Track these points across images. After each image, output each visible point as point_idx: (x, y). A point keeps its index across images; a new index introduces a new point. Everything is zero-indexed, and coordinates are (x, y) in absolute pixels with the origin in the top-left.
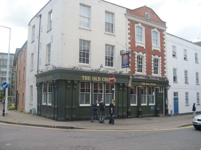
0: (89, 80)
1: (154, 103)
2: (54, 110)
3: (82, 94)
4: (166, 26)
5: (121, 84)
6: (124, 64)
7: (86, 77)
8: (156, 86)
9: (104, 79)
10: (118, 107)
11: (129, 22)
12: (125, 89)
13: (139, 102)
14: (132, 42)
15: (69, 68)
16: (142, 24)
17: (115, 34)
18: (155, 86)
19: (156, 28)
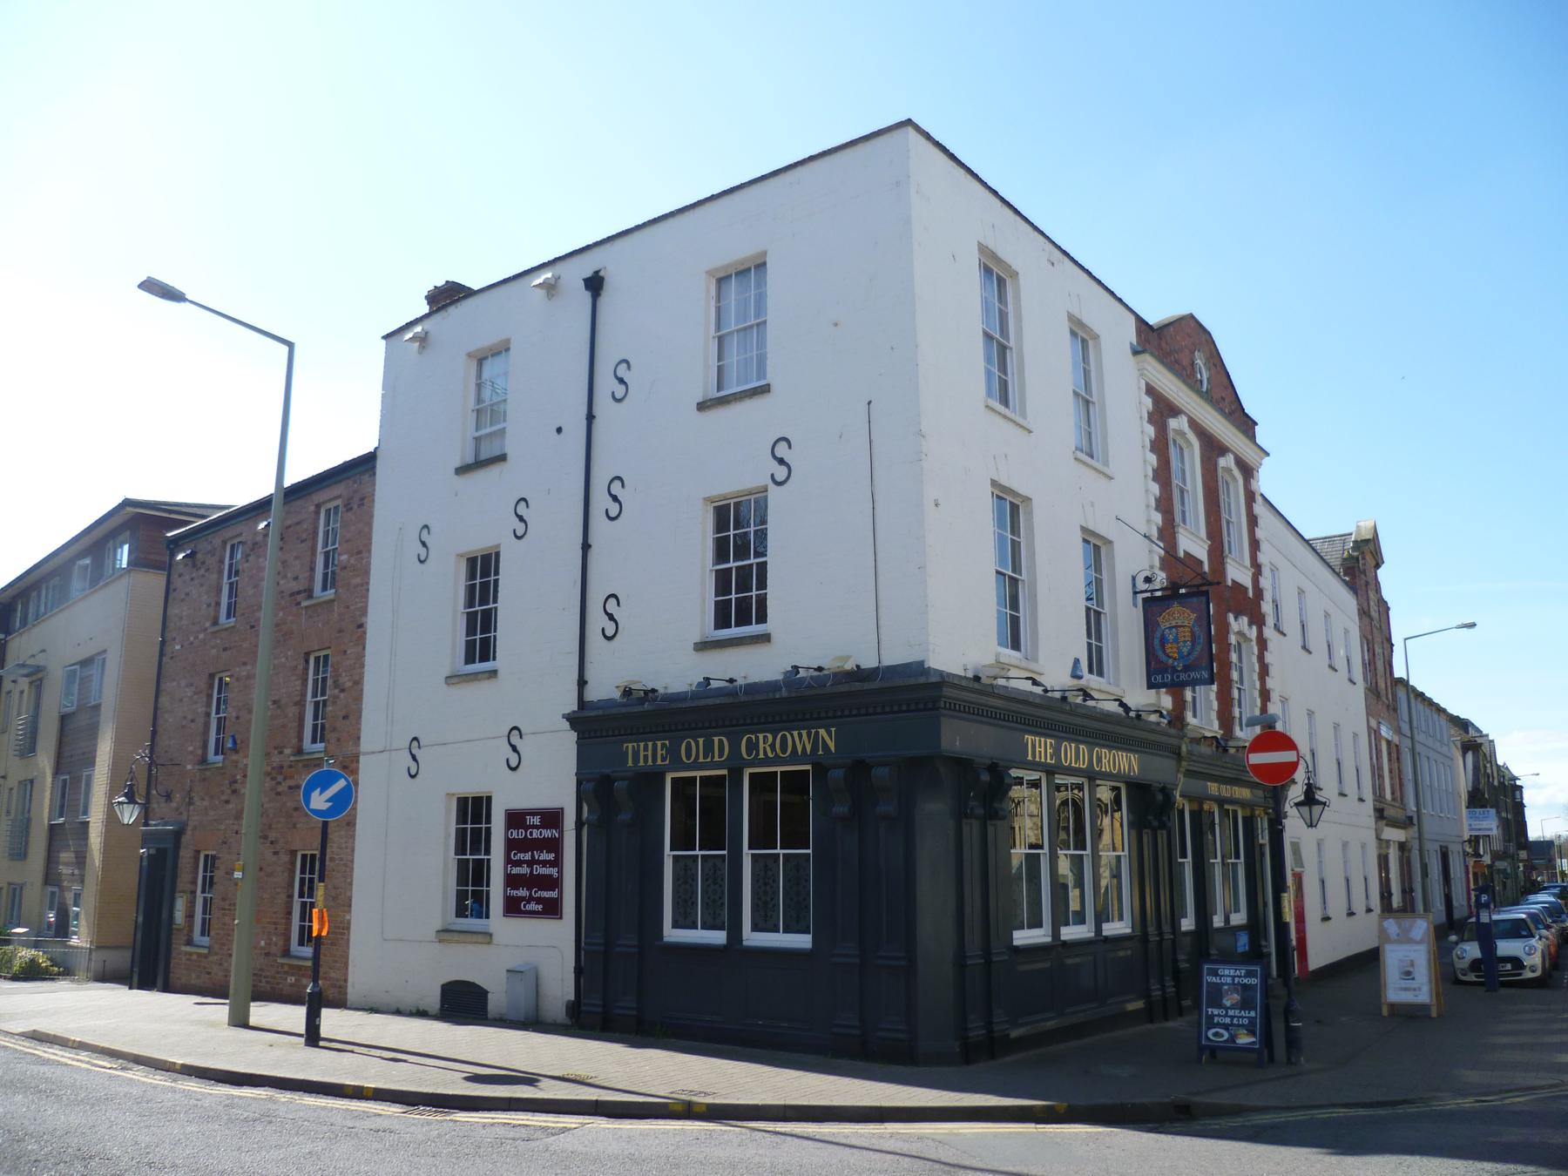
1: (1040, 925)
7: (1037, 739)
9: (1099, 760)
14: (1168, 534)
16: (1194, 425)
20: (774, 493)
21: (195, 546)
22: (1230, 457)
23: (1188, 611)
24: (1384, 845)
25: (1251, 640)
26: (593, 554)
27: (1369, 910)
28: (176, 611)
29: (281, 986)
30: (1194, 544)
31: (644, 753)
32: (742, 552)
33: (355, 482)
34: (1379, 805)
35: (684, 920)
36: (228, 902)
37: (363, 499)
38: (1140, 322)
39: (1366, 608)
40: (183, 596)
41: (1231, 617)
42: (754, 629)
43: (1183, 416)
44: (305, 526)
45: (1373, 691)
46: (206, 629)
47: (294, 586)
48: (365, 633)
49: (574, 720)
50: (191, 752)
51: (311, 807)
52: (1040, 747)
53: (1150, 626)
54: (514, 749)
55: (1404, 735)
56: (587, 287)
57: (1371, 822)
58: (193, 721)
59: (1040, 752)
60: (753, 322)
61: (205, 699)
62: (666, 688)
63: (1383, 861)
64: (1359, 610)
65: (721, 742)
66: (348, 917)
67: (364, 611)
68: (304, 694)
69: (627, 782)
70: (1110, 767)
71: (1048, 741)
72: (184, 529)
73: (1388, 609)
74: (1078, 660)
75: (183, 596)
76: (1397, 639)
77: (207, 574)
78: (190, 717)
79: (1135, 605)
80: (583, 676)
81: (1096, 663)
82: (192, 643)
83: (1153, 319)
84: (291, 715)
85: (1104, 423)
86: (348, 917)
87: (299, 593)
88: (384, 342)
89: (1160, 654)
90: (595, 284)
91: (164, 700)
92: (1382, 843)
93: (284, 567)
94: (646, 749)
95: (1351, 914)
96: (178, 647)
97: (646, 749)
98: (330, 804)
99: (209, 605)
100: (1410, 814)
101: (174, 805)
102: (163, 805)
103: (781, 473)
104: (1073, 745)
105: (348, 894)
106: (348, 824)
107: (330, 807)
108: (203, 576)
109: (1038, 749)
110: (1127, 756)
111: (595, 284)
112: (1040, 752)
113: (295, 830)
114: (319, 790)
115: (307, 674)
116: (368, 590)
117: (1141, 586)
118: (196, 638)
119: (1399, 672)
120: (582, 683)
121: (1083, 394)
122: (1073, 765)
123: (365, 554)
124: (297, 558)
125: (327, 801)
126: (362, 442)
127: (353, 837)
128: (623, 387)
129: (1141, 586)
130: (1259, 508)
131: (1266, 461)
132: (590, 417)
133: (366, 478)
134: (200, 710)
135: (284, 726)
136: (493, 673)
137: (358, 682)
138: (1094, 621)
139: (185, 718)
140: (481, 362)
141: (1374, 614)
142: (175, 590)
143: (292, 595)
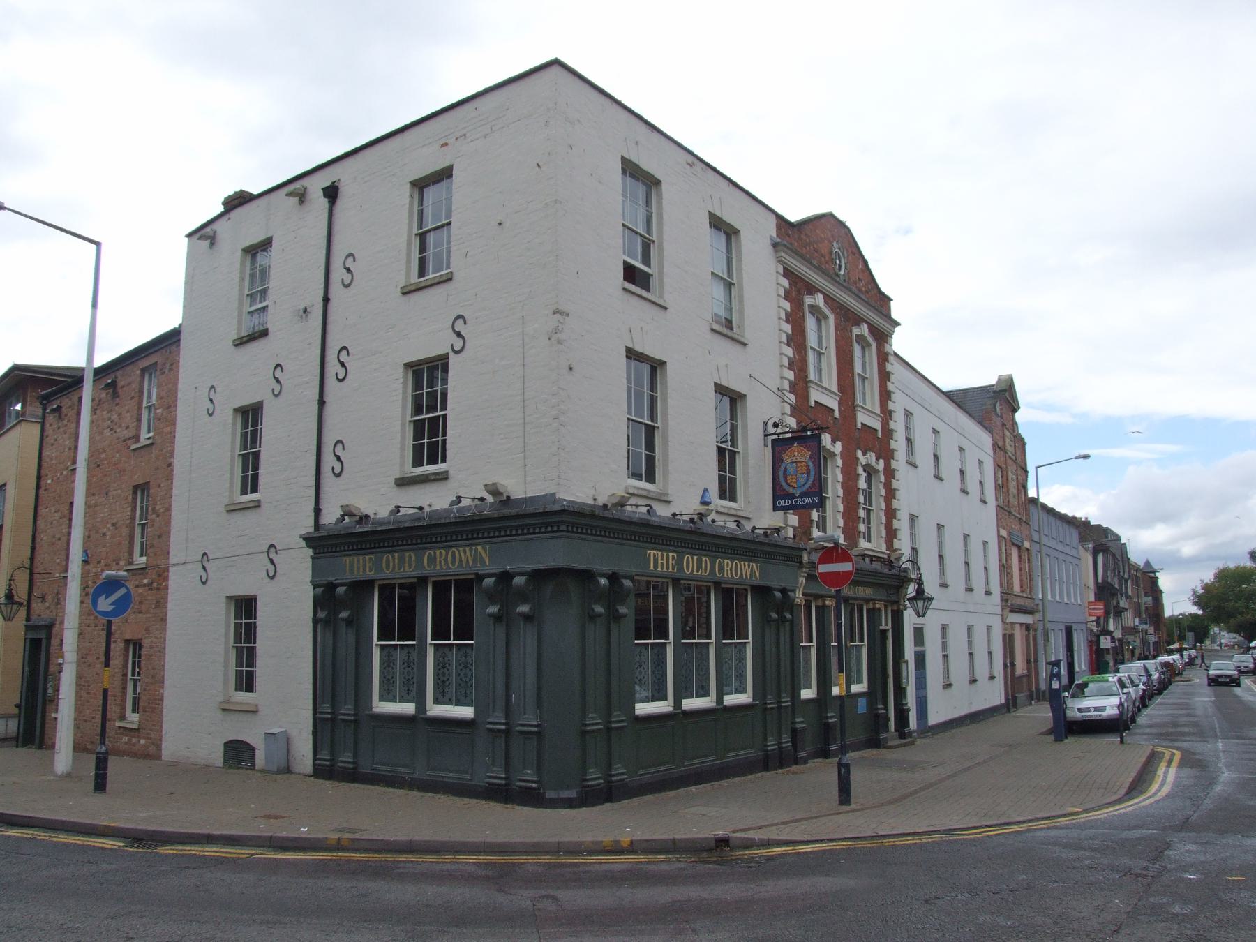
0: (670, 570)
1: (664, 698)
2: (609, 740)
3: (387, 650)
4: (894, 315)
5: (603, 575)
6: (791, 490)
7: (660, 553)
8: (873, 600)
9: (721, 568)
10: (584, 733)
11: (786, 283)
12: (622, 610)
13: (824, 685)
14: (800, 386)
15: (590, 502)
16: (827, 298)
17: (661, 296)
18: (868, 601)
19: (867, 323)
20: (453, 360)
21: (60, 403)
22: (865, 327)
23: (805, 450)
24: (1009, 626)
25: (879, 472)
26: (329, 409)
27: (992, 678)
28: (48, 453)
29: (118, 744)
30: (825, 395)
31: (360, 567)
32: (432, 408)
33: (166, 351)
34: (1005, 596)
35: (387, 695)
36: (83, 680)
37: (172, 365)
38: (780, 218)
39: (1000, 444)
40: (52, 441)
41: (859, 453)
42: (439, 467)
43: (819, 294)
44: (134, 386)
45: (1003, 510)
46: (68, 467)
47: (127, 434)
48: (172, 470)
49: (309, 540)
50: (58, 564)
51: (98, 609)
52: (662, 559)
53: (776, 461)
54: (272, 562)
55: (1035, 542)
56: (325, 196)
57: (998, 609)
58: (59, 539)
59: (662, 564)
60: (444, 222)
61: (67, 522)
62: (375, 514)
63: (1008, 640)
64: (993, 445)
65: (410, 556)
66: (161, 691)
67: (172, 455)
68: (133, 518)
69: (322, 589)
70: (731, 573)
71: (671, 555)
72: (47, 391)
73: (1024, 444)
74: (707, 490)
75: (52, 441)
76: (1030, 468)
77: (68, 424)
78: (58, 536)
79: (766, 445)
80: (318, 505)
81: (727, 489)
82: (59, 478)
83: (793, 216)
84: (124, 534)
85: (741, 302)
86: (161, 691)
87: (129, 439)
88: (187, 239)
89: (783, 483)
90: (332, 193)
91: (41, 523)
92: (1008, 626)
93: (120, 419)
94: (358, 561)
95: (973, 681)
96: (49, 481)
97: (358, 561)
98: (114, 607)
99: (70, 449)
100: (1037, 602)
101: (47, 604)
102: (39, 604)
103: (458, 344)
104: (695, 557)
105: (162, 673)
106: (162, 620)
107: (114, 609)
108: (66, 425)
109: (660, 561)
110: (749, 565)
111: (332, 193)
112: (662, 564)
113: (127, 624)
114: (104, 596)
115: (136, 503)
116: (174, 437)
117: (771, 430)
118: (62, 474)
119: (1032, 493)
120: (318, 511)
121: (725, 277)
122: (695, 573)
123: (174, 409)
124: (128, 412)
125: (111, 604)
126: (168, 317)
127: (165, 630)
128: (350, 275)
129: (771, 430)
130: (892, 367)
131: (897, 329)
132: (326, 300)
133: (174, 348)
134: (64, 531)
135: (120, 544)
136: (257, 505)
137: (168, 509)
138: (727, 458)
139: (54, 537)
140: (254, 256)
141: (1009, 448)
142: (47, 437)
143: (124, 441)
